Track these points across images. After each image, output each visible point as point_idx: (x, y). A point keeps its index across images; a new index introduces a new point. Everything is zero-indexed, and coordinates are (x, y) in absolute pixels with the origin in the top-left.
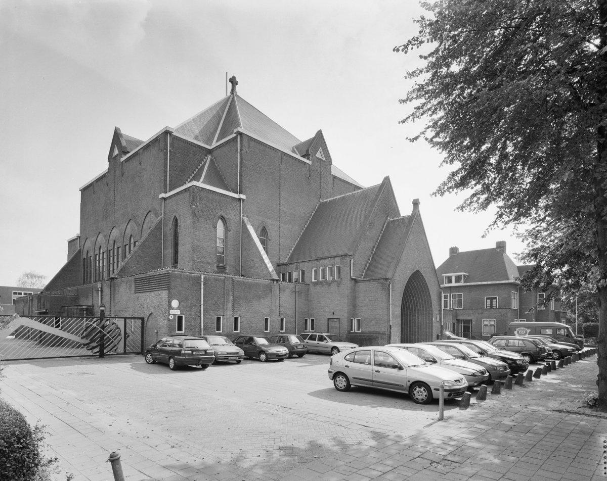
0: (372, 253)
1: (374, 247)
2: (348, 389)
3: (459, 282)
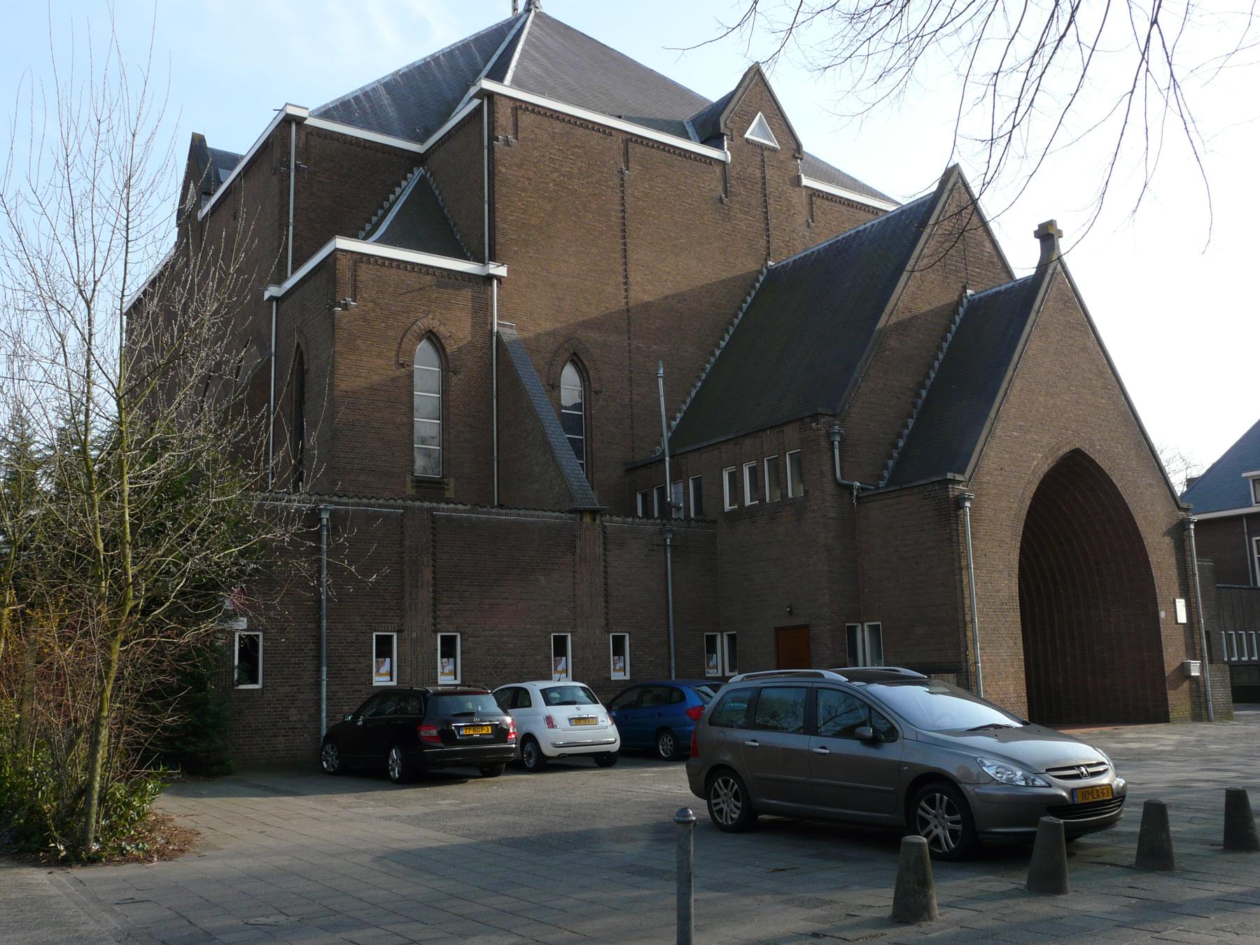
0: (914, 405)
1: (921, 385)
2: (748, 824)
3: (222, 183)
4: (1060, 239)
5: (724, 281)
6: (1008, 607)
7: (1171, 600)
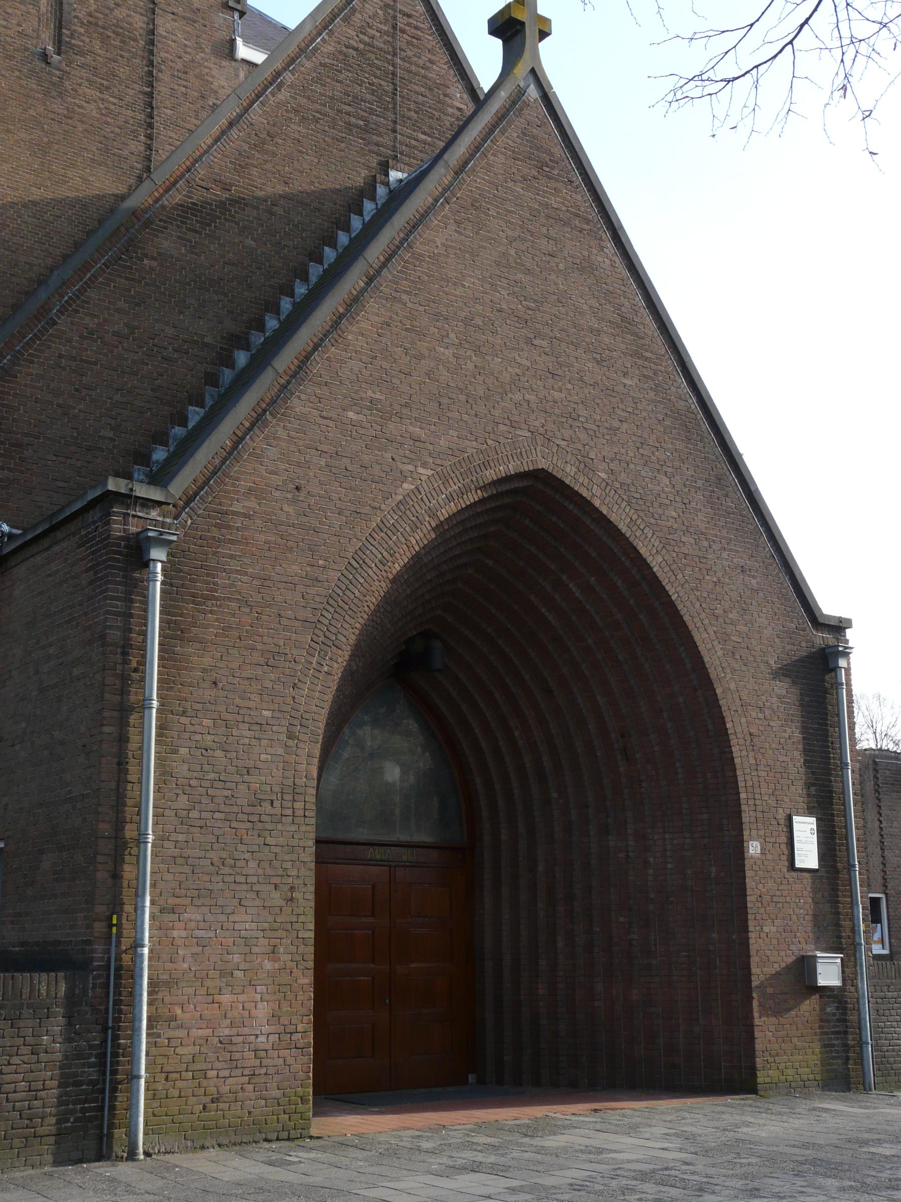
4: (544, 47)
5: (34, 203)
6: (277, 811)
7: (781, 815)
